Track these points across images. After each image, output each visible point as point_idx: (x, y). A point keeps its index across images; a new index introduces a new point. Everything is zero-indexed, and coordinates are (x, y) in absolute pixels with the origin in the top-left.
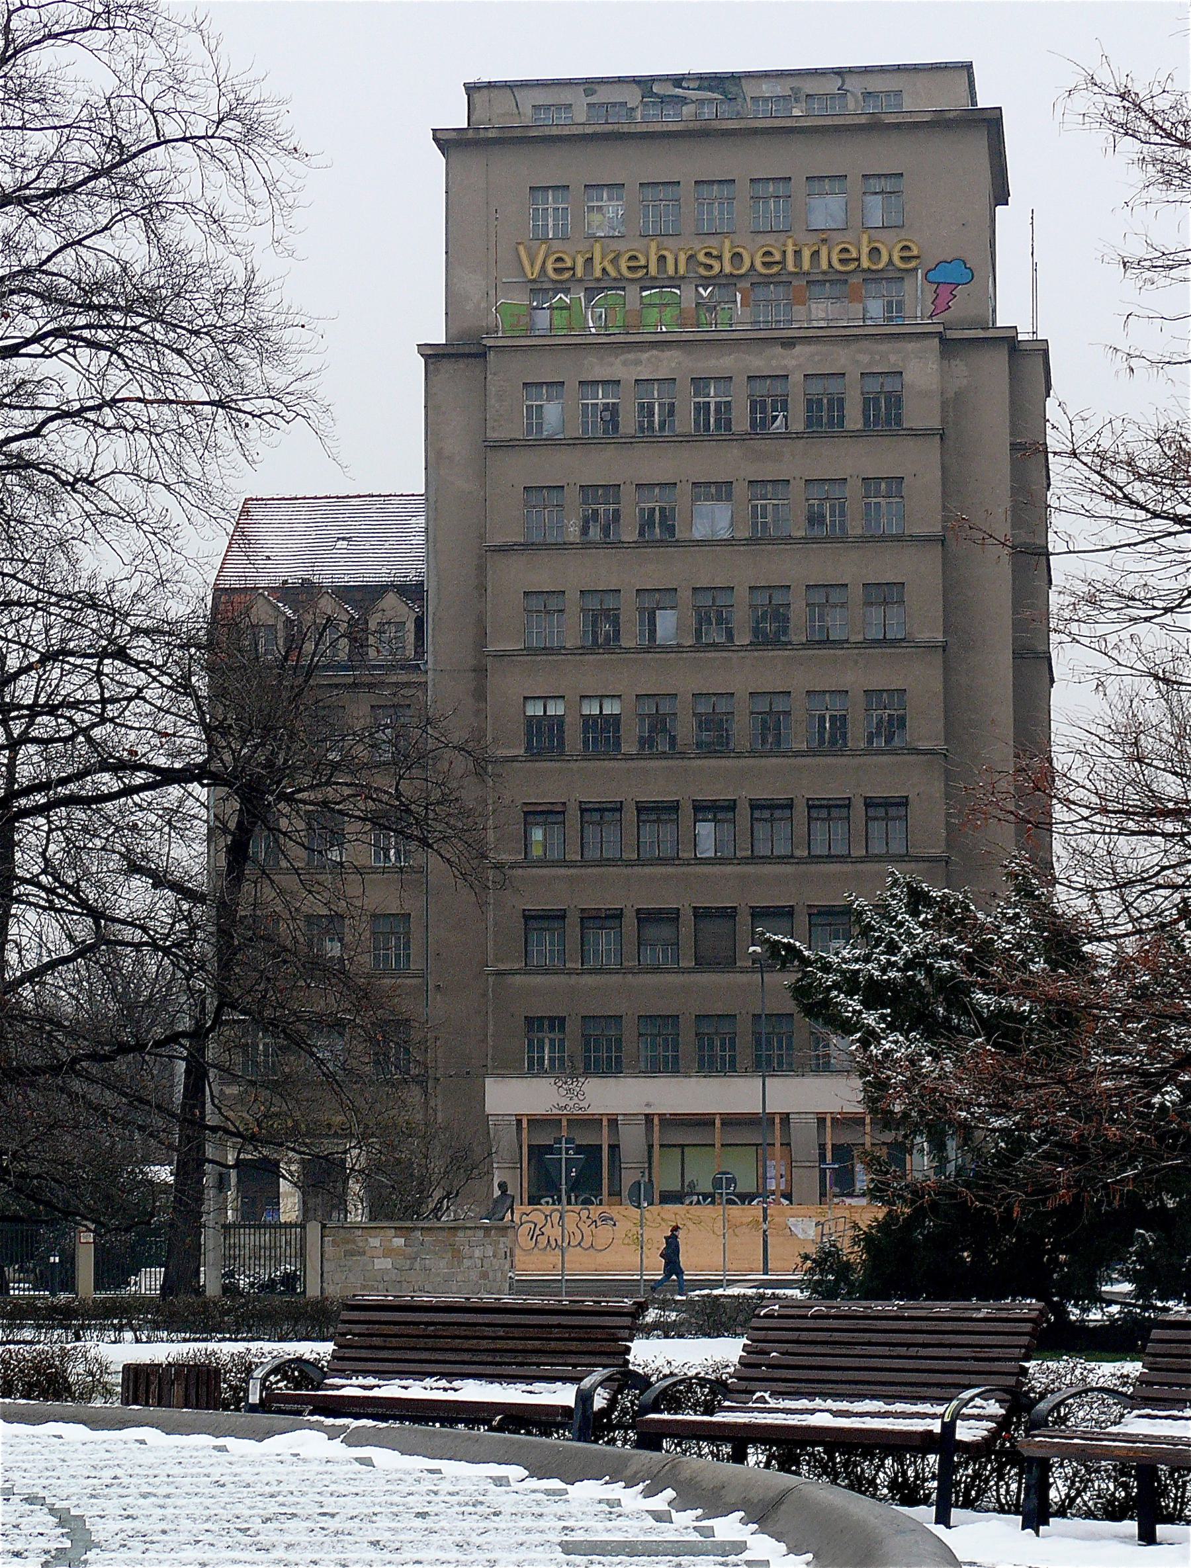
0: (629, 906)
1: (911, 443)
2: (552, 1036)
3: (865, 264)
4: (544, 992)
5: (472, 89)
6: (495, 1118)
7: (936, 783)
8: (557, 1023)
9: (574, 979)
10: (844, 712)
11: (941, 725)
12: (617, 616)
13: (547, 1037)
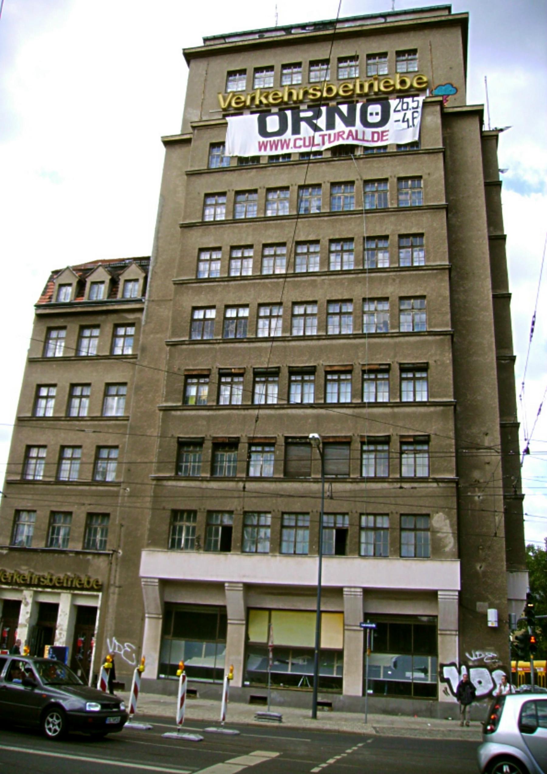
1: (426, 157)
2: (188, 524)
3: (398, 87)
4: (186, 491)
5: (206, 40)
6: (145, 580)
7: (447, 354)
8: (192, 514)
9: (205, 485)
11: (449, 317)
13: (185, 524)
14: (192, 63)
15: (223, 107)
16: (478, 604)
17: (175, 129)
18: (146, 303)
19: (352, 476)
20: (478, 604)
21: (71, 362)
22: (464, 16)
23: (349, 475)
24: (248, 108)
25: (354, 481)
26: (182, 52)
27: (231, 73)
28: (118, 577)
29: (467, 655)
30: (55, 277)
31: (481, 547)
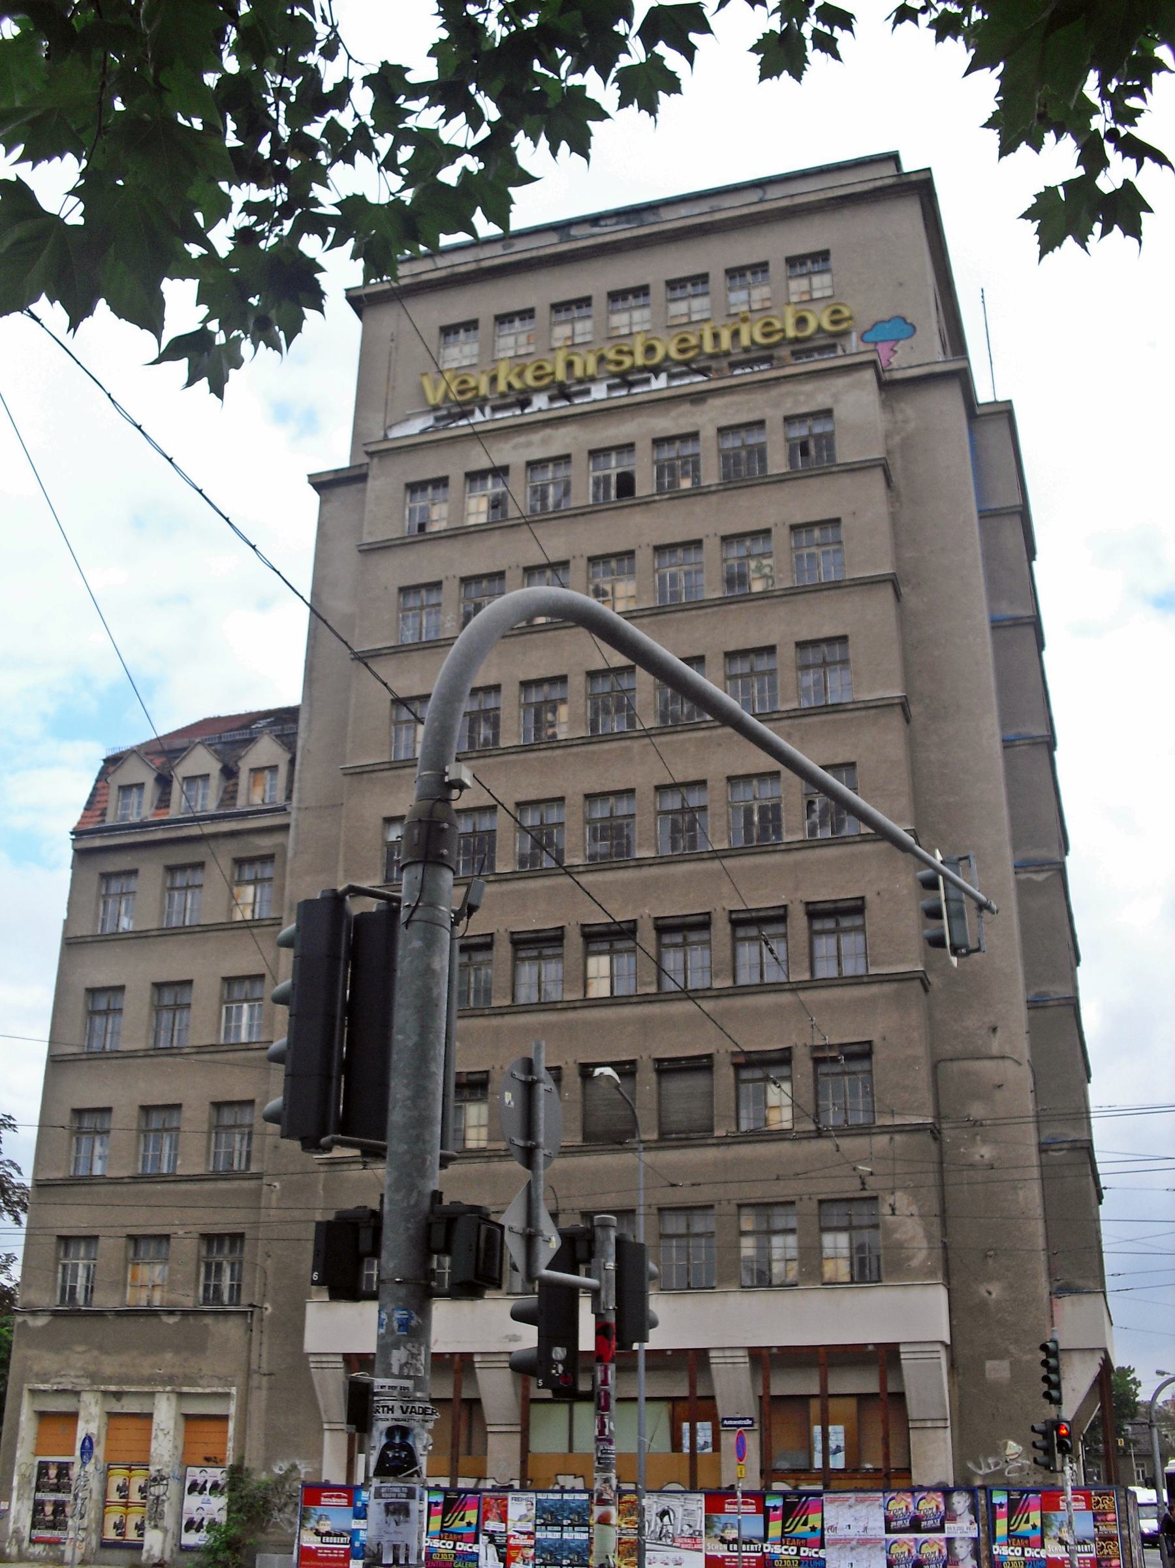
0: (497, 1067)
1: (846, 480)
3: (791, 333)
10: (774, 801)
12: (497, 718)
14: (368, 313)
15: (432, 401)
16: (989, 1364)
17: (338, 455)
18: (294, 815)
19: (717, 1134)
20: (989, 1364)
21: (151, 940)
22: (922, 176)
23: (712, 1130)
24: (485, 400)
25: (723, 1142)
26: (344, 294)
27: (448, 331)
28: (265, 1355)
29: (970, 1465)
30: (111, 769)
31: (991, 1253)
